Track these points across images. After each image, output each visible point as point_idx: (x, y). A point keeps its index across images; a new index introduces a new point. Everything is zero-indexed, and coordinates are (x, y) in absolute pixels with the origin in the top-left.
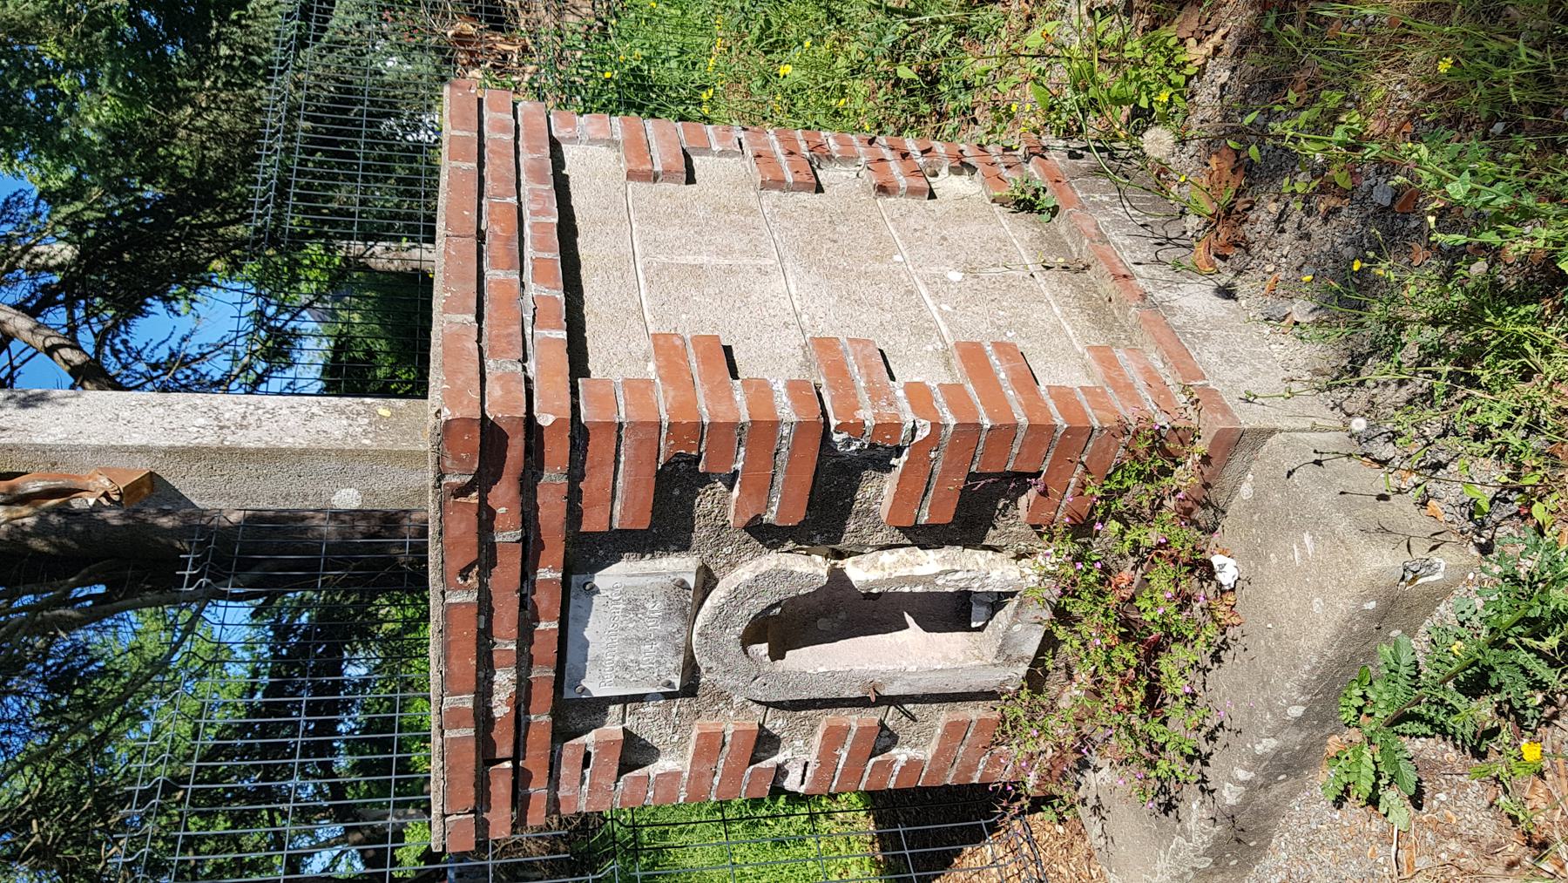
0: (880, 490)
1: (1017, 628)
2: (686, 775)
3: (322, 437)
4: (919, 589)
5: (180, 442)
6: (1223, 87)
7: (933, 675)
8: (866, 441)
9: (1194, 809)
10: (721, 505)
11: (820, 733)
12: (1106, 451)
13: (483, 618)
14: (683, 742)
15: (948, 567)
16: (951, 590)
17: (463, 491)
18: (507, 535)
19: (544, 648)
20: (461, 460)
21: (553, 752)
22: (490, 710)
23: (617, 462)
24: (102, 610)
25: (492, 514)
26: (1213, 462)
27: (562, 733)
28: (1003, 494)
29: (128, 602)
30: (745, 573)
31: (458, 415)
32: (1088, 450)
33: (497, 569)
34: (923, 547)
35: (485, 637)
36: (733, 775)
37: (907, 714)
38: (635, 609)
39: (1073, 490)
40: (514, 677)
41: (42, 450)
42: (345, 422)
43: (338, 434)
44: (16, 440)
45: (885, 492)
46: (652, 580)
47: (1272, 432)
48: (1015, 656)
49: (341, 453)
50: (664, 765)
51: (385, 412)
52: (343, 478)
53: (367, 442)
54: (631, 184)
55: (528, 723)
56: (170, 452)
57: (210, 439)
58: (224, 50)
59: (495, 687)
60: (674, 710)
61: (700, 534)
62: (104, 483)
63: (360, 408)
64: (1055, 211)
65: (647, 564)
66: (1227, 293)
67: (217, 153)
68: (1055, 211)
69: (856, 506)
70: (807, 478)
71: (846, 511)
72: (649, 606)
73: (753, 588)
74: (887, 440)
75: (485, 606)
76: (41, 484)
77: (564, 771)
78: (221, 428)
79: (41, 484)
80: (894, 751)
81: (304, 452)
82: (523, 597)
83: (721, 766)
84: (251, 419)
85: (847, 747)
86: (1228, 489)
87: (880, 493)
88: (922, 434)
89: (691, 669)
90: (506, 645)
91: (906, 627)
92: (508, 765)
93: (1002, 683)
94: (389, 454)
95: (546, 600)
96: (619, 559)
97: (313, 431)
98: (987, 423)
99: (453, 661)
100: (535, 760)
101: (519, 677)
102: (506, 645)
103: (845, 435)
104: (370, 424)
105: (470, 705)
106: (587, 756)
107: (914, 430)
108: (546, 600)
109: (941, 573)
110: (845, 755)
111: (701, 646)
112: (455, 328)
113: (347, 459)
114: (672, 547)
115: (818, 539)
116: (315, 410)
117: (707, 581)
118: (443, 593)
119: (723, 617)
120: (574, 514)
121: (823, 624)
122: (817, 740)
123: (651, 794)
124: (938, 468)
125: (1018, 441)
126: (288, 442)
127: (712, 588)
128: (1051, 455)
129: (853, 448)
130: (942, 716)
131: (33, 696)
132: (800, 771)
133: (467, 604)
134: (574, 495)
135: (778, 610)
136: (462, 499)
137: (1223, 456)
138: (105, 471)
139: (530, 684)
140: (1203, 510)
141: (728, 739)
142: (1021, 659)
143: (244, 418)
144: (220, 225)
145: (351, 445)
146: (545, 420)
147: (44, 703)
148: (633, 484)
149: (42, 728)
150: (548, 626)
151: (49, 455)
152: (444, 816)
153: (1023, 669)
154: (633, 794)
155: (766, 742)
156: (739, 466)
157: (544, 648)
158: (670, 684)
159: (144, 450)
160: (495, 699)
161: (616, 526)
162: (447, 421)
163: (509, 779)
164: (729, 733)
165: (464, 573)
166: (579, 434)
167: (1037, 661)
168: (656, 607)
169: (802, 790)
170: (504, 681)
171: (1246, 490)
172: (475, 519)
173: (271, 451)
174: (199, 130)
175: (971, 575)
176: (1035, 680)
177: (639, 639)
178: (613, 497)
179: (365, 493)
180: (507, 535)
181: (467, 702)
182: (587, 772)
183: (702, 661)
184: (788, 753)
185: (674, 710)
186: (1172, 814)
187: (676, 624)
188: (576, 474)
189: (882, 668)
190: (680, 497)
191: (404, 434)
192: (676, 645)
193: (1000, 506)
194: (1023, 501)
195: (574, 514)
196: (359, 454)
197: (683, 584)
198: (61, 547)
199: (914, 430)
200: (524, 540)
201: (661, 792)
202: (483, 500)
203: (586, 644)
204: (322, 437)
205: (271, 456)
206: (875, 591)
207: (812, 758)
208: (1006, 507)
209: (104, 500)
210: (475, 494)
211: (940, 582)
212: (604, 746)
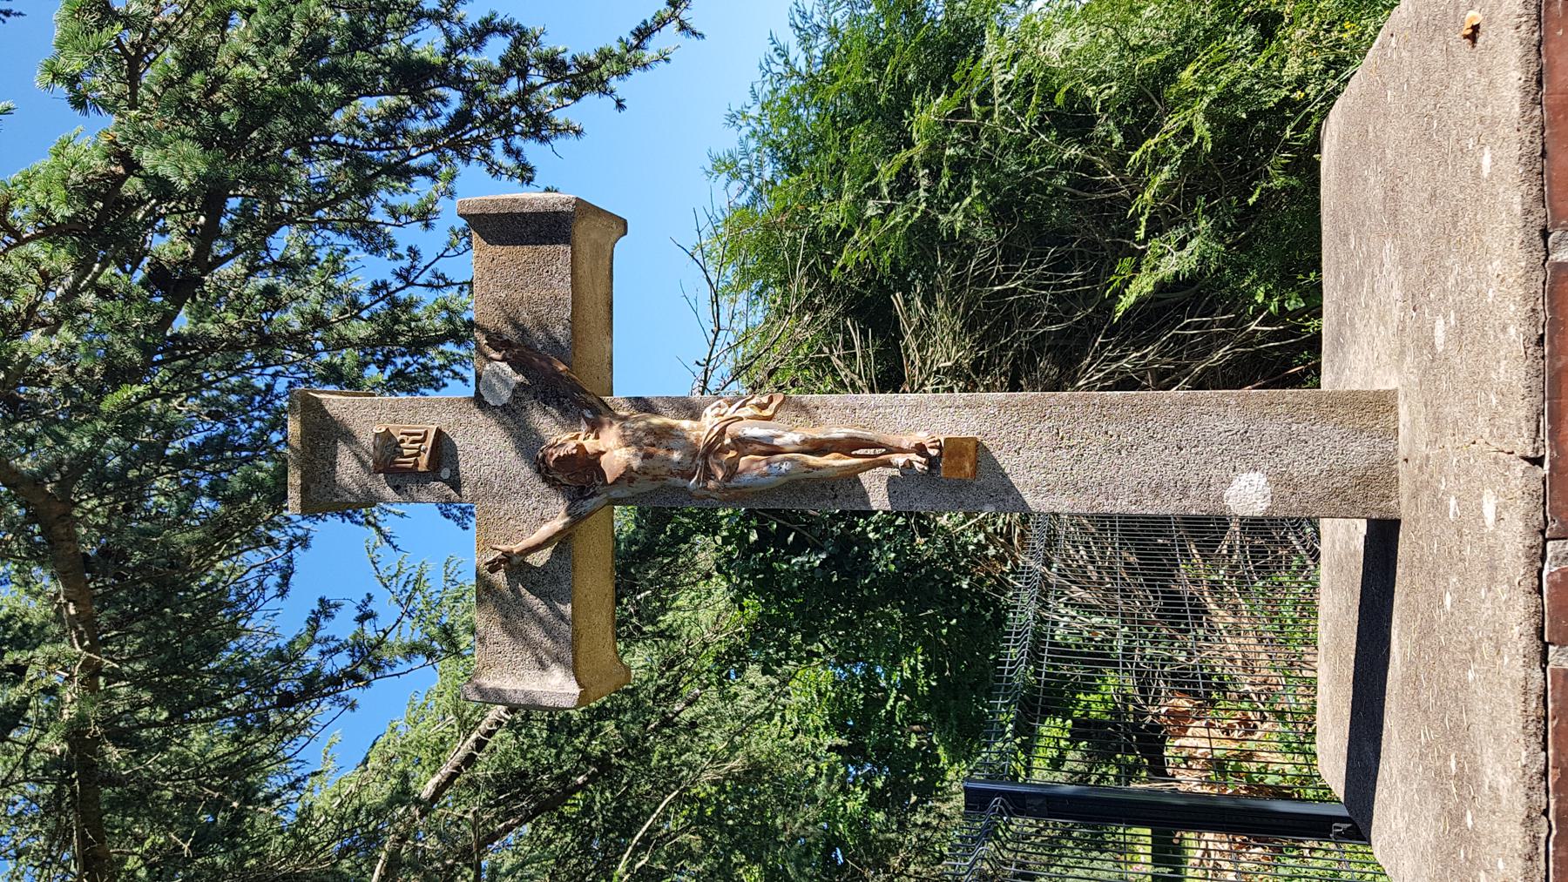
62: (921, 437)
118: (1545, 234)
179: (1282, 482)
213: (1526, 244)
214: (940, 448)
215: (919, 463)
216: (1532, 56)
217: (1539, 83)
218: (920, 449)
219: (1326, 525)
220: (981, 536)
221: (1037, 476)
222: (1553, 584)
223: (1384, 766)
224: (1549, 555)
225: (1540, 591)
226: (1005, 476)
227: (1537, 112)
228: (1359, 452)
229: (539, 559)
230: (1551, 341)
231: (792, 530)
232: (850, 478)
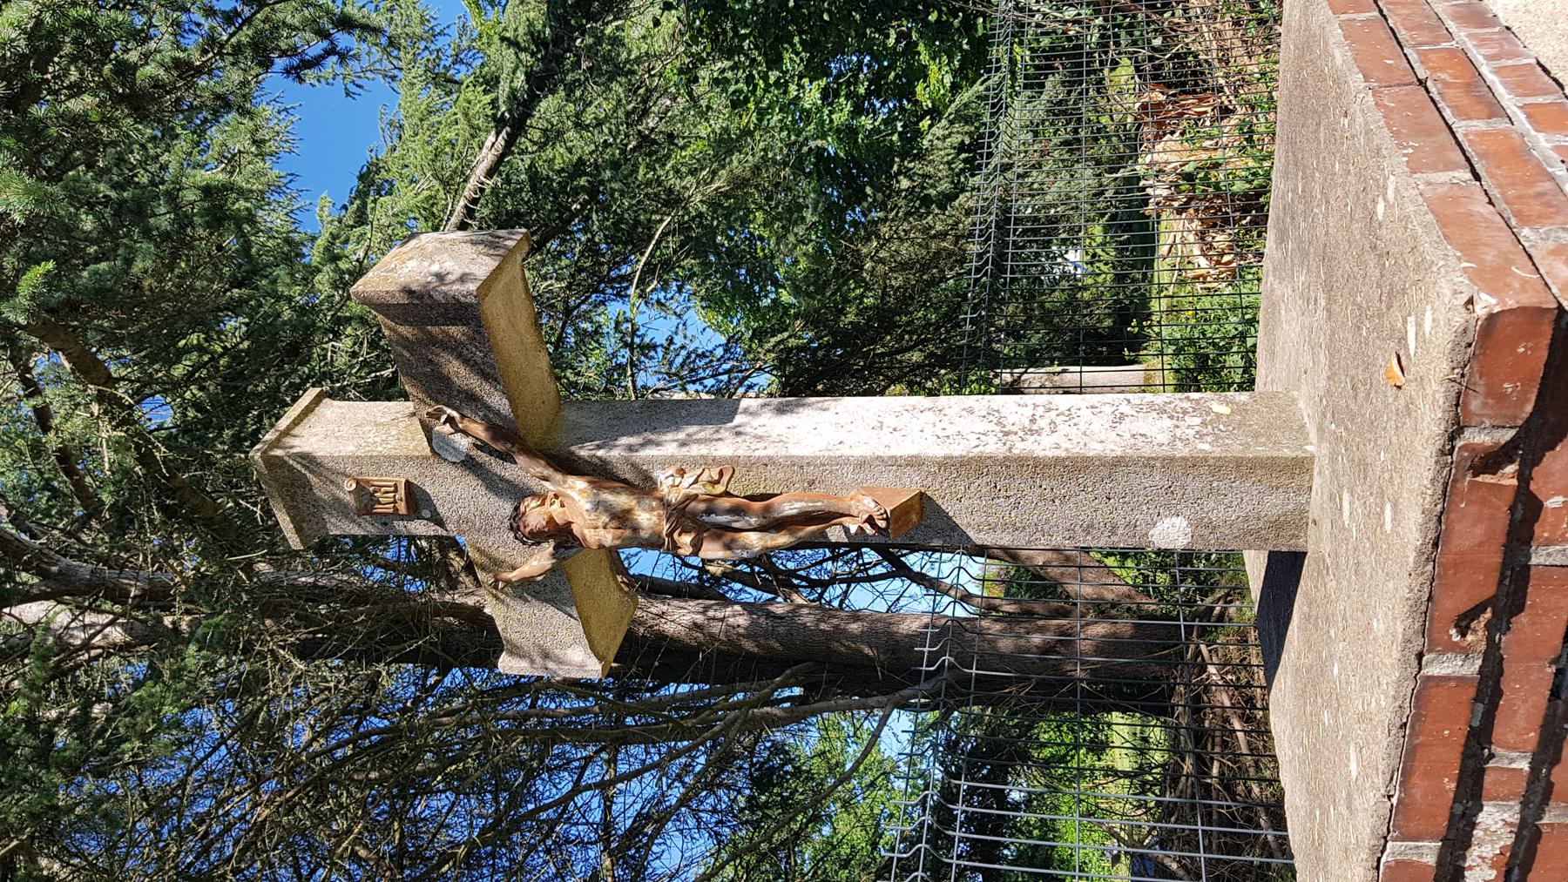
3: (1140, 441)
5: (958, 450)
13: (1480, 707)
17: (1490, 461)
20: (1501, 397)
24: (800, 712)
29: (823, 704)
31: (1511, 303)
33: (1523, 618)
35: (1479, 740)
40: (1516, 819)
41: (799, 464)
42: (1168, 423)
43: (1163, 438)
44: (771, 452)
49: (1169, 462)
51: (1225, 410)
52: (1169, 502)
53: (1206, 447)
56: (946, 464)
57: (993, 447)
58: (905, 183)
59: (1477, 833)
62: (867, 505)
63: (1186, 405)
67: (897, 281)
75: (1489, 688)
76: (798, 505)
78: (1006, 434)
79: (798, 505)
81: (1118, 462)
84: (1043, 423)
94: (1238, 463)
97: (1127, 435)
101: (1523, 820)
104: (1204, 423)
105: (1430, 859)
112: (1440, 190)
113: (1176, 473)
116: (1124, 408)
118: (1420, 656)
126: (1095, 449)
131: (739, 792)
133: (1461, 680)
136: (1487, 478)
138: (870, 491)
139: (1537, 835)
143: (1033, 421)
144: (899, 352)
145: (1182, 451)
147: (750, 799)
149: (747, 822)
151: (806, 470)
159: (915, 462)
162: (1491, 318)
172: (1503, 516)
174: (882, 261)
179: (1197, 524)
191: (1256, 436)
196: (1193, 464)
198: (769, 649)
202: (1524, 478)
204: (1140, 441)
205: (1073, 468)
209: (867, 527)
210: (1511, 469)
213: (1404, 661)
214: (887, 519)
216: (1432, 525)
217: (1436, 545)
219: (1246, 553)
221: (978, 518)
222: (1388, 867)
223: (1284, 656)
224: (1388, 850)
225: (1378, 868)
226: (950, 518)
227: (1430, 567)
228: (1274, 504)
230: (1412, 727)
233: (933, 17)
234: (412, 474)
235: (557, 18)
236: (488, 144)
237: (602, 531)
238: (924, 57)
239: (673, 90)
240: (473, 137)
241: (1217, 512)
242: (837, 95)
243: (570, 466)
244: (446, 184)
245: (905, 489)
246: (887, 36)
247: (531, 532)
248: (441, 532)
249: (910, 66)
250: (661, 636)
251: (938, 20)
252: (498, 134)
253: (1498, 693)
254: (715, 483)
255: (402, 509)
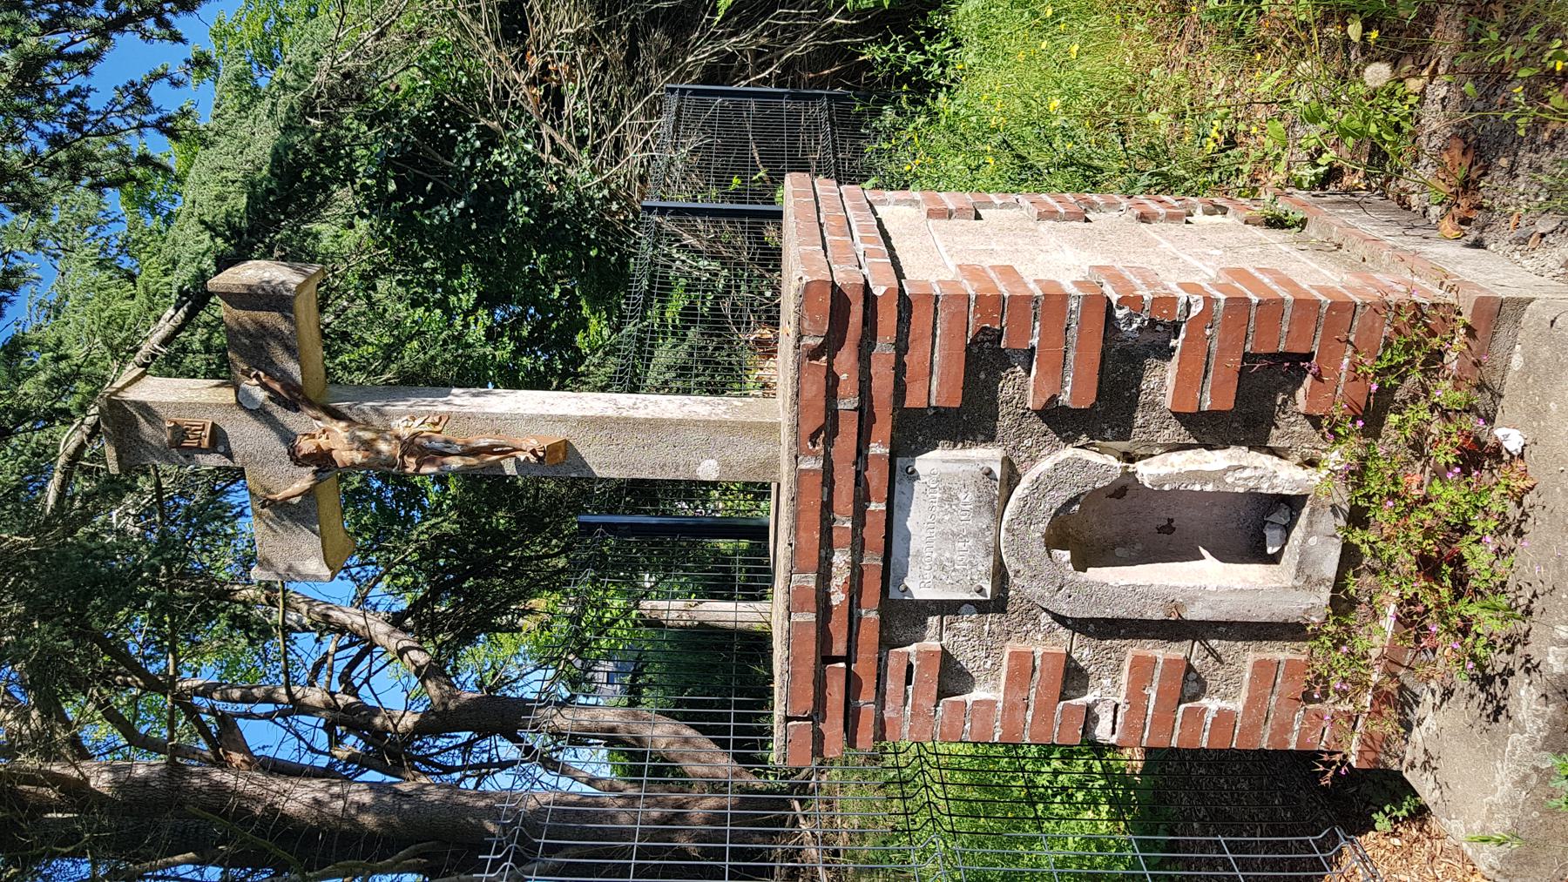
0: (1163, 380)
1: (1313, 541)
2: (1000, 705)
4: (1209, 488)
6: (1443, 99)
7: (1234, 597)
8: (1146, 316)
9: (1525, 697)
10: (1022, 390)
11: (1126, 667)
12: (1372, 329)
14: (996, 666)
15: (1235, 463)
16: (1241, 490)
17: (815, 354)
18: (847, 403)
19: (874, 533)
20: (816, 322)
21: (880, 659)
22: (828, 595)
23: (934, 335)
25: (836, 379)
26: (1478, 334)
27: (887, 642)
28: (1280, 387)
30: (1045, 465)
32: (1354, 330)
33: (838, 439)
34: (1209, 448)
36: (1044, 711)
37: (1212, 652)
38: (950, 499)
39: (1345, 373)
45: (1168, 382)
46: (964, 467)
47: (1532, 300)
48: (1314, 579)
50: (978, 694)
52: (706, 451)
54: (931, 222)
55: (860, 618)
60: (986, 628)
61: (1004, 422)
62: (533, 443)
64: (1304, 222)
65: (958, 453)
66: (1478, 244)
68: (1304, 222)
69: (1142, 398)
70: (1096, 356)
71: (1133, 404)
72: (962, 496)
73: (1053, 480)
74: (1164, 316)
75: (828, 477)
77: (890, 685)
80: (1204, 701)
82: (858, 473)
83: (1033, 697)
85: (1155, 684)
86: (1499, 367)
87: (1163, 382)
88: (1196, 310)
89: (1000, 574)
90: (844, 523)
91: (1203, 558)
92: (842, 665)
93: (1306, 612)
94: (743, 425)
95: (876, 477)
96: (935, 447)
98: (1255, 300)
99: (802, 534)
100: (864, 667)
101: (853, 562)
102: (844, 523)
103: (1126, 311)
105: (813, 585)
106: (910, 667)
107: (1188, 305)
108: (876, 477)
109: (1229, 469)
110: (1153, 696)
111: (1010, 544)
114: (981, 437)
115: (1108, 434)
117: (1011, 478)
119: (1028, 512)
120: (900, 390)
121: (1119, 552)
122: (1124, 678)
123: (968, 726)
124: (1214, 346)
125: (1287, 318)
127: (1016, 485)
128: (1320, 333)
129: (1135, 326)
130: (1248, 656)
132: (1110, 716)
134: (900, 368)
135: (1077, 507)
137: (1487, 329)
140: (1485, 395)
141: (1038, 662)
142: (1321, 582)
144: (547, 556)
145: (714, 418)
146: (878, 291)
148: (947, 358)
150: (877, 506)
152: (788, 719)
153: (1326, 594)
154: (951, 724)
155: (1074, 677)
156: (1035, 341)
157: (874, 533)
158: (981, 591)
160: (834, 582)
161: (933, 403)
163: (842, 681)
164: (1038, 654)
165: (813, 438)
166: (905, 304)
167: (1339, 584)
168: (967, 497)
169: (1113, 740)
170: (841, 559)
171: (1517, 362)
172: (823, 382)
173: (656, 420)
175: (1259, 473)
176: (1342, 604)
177: (953, 534)
178: (931, 373)
179: (725, 465)
180: (847, 403)
181: (811, 582)
182: (910, 688)
183: (1011, 563)
184: (1097, 693)
185: (986, 628)
186: (1502, 718)
187: (986, 520)
188: (901, 346)
189: (1182, 584)
190: (985, 381)
192: (986, 544)
193: (1279, 401)
194: (1300, 393)
195: (900, 390)
197: (989, 473)
199: (1188, 305)
200: (860, 409)
201: (977, 725)
203: (908, 537)
206: (1167, 488)
207: (1121, 700)
208: (1285, 402)
211: (1229, 480)
212: (926, 656)
215: (533, 459)
218: (533, 452)
220: (606, 192)
229: (296, 500)
231: (430, 180)
232: (498, 465)
233: (593, 253)
234: (217, 417)
235: (256, 212)
236: (167, 316)
237: (354, 453)
238: (586, 312)
239: (351, 293)
240: (150, 309)
241: (734, 457)
242: (501, 335)
243: (337, 415)
244: (115, 351)
245: (558, 435)
246: (553, 290)
247: (305, 456)
248: (229, 463)
249: (572, 318)
250: (286, 818)
251: (598, 256)
252: (177, 309)
253: (833, 482)
254: (436, 424)
255: (205, 443)
